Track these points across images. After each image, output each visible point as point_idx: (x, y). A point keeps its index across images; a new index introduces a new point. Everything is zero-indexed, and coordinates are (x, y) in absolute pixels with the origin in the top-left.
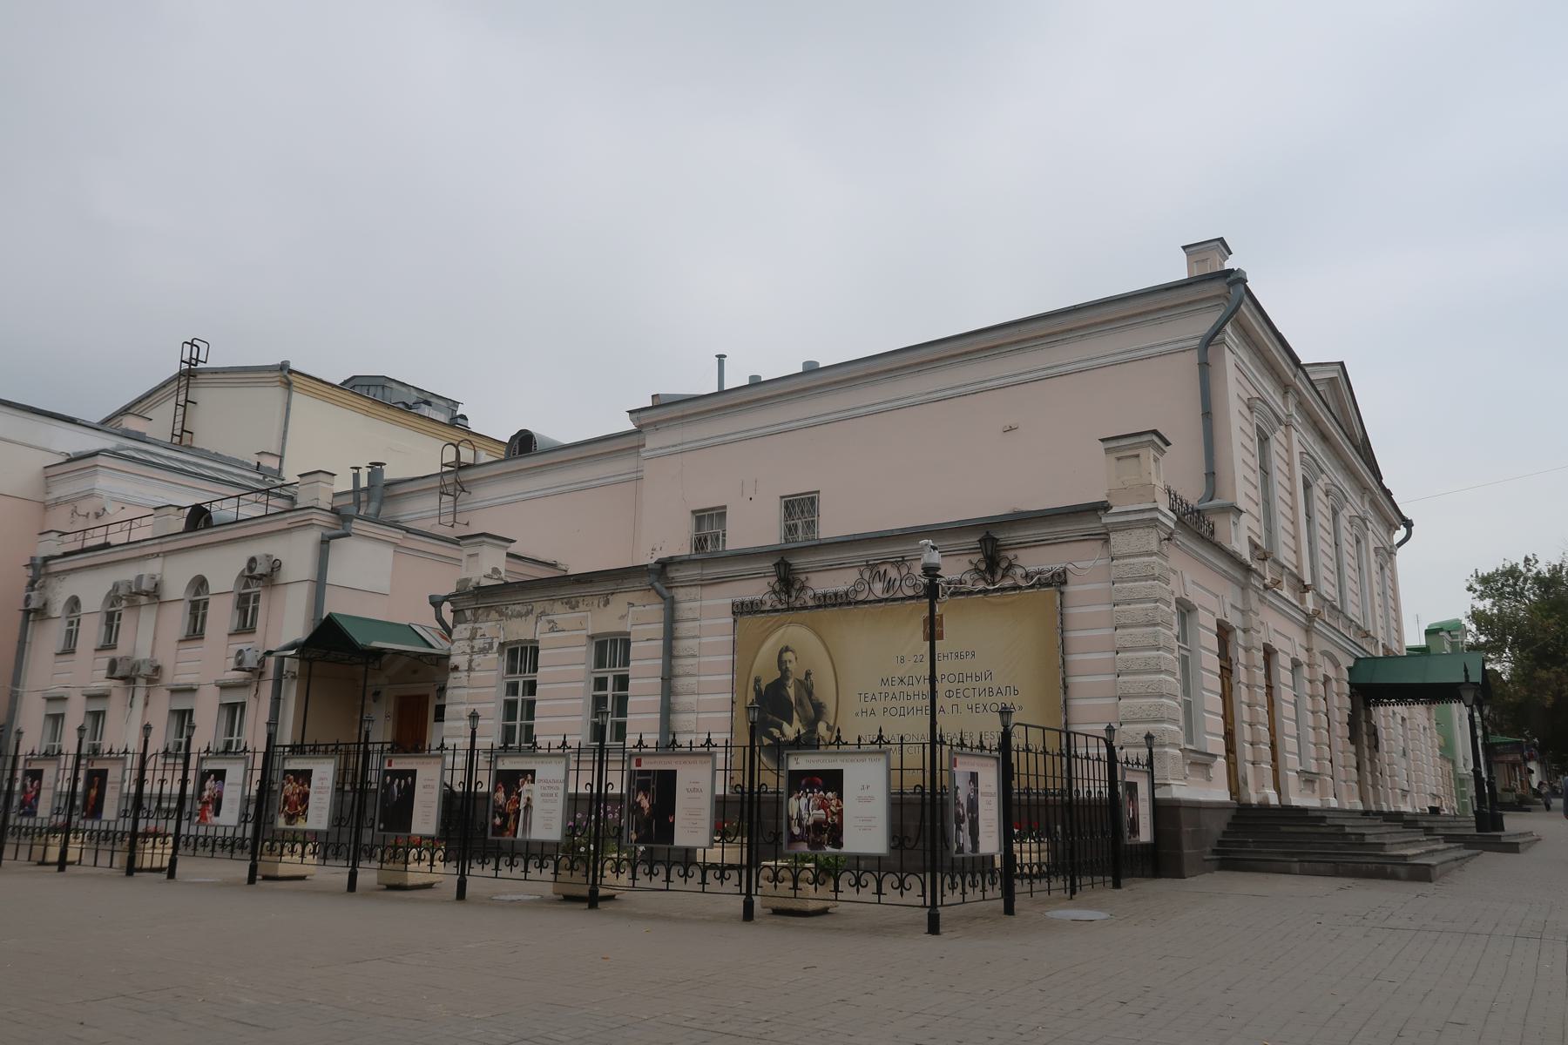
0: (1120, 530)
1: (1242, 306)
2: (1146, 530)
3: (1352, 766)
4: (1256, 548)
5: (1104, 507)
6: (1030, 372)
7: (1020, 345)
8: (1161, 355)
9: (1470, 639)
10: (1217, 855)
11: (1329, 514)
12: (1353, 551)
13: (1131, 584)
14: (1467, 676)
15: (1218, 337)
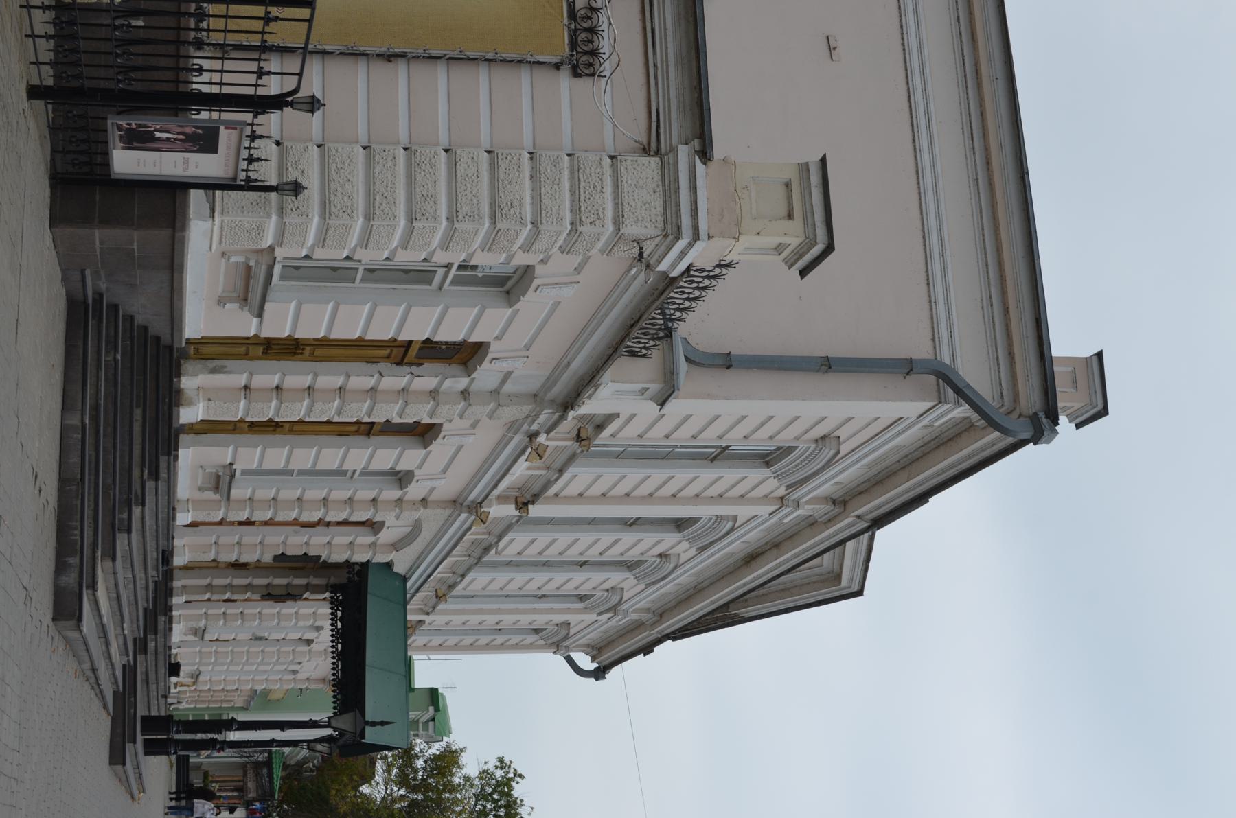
0: (663, 176)
1: (997, 434)
2: (660, 219)
3: (240, 554)
4: (599, 426)
5: (705, 154)
6: (925, 90)
7: (972, 77)
8: (931, 303)
9: (419, 744)
10: (94, 299)
11: (633, 555)
12: (569, 589)
13: (567, 185)
14: (374, 724)
15: (950, 392)
